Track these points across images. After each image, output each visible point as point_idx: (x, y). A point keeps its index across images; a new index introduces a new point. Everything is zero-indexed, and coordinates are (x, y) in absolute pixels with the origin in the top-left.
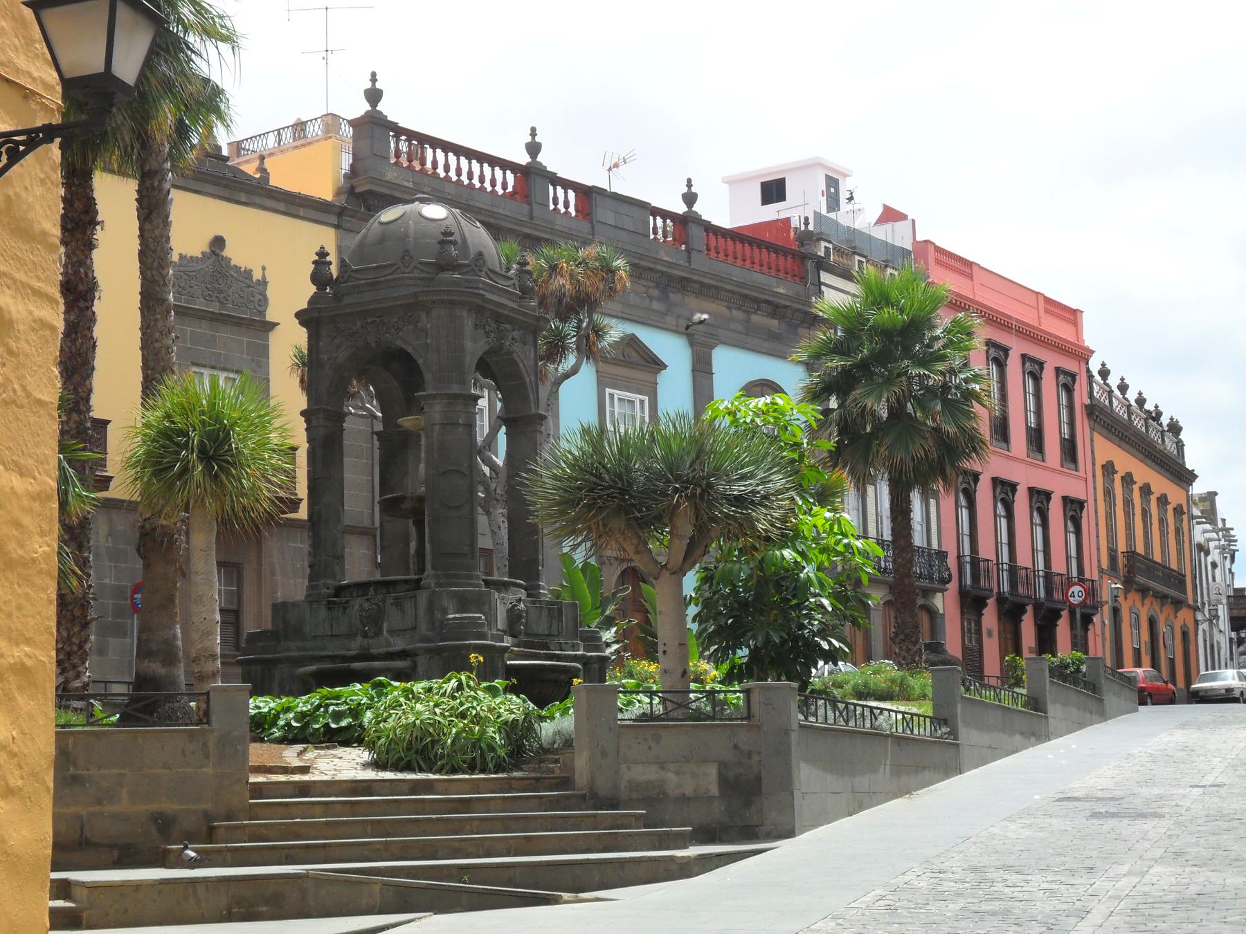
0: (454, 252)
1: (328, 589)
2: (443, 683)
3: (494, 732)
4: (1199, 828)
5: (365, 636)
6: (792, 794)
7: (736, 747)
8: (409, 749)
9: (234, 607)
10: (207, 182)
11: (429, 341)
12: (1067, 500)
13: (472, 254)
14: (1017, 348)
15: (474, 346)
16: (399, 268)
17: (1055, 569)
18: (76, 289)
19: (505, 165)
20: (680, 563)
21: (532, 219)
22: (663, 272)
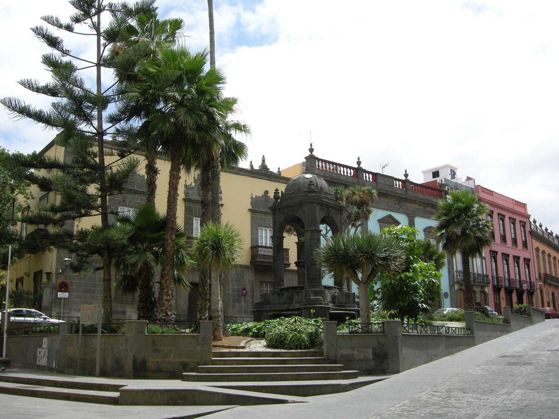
0: (313, 187)
2: (290, 320)
3: (305, 336)
4: (542, 370)
5: (288, 303)
6: (399, 358)
7: (378, 342)
8: (276, 341)
12: (525, 259)
14: (496, 211)
15: (320, 215)
17: (522, 279)
19: (350, 168)
21: (359, 182)
22: (398, 197)
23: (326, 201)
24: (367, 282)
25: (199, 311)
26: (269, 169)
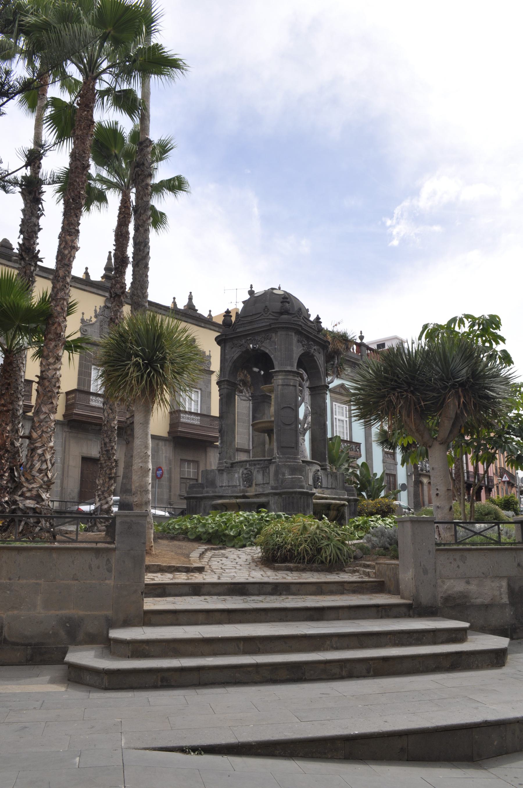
1: (227, 464)
9: (196, 478)
10: (190, 318)
11: (276, 347)
13: (296, 309)
16: (263, 314)
20: (446, 436)
25: (99, 495)
26: (197, 310)
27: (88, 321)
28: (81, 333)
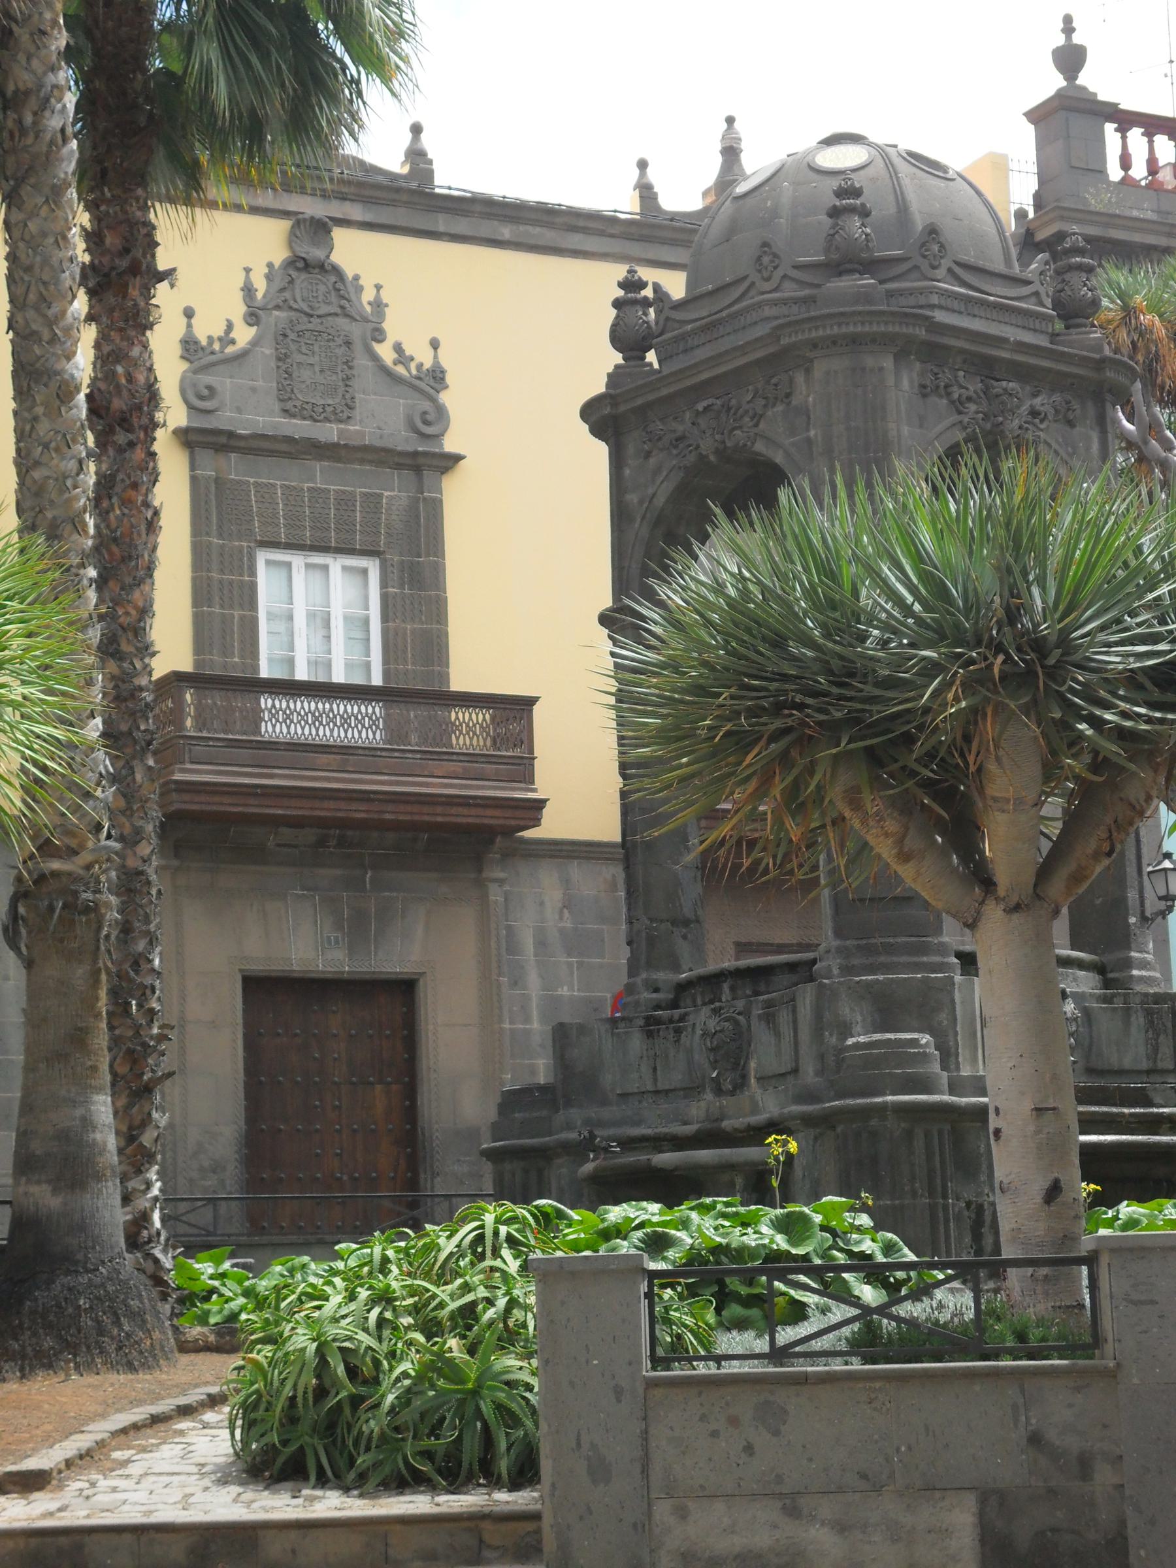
1: (656, 990)
5: (719, 1091)
7: (1035, 1440)
16: (753, 284)
18: (108, 409)
23: (976, 325)
24: (1037, 896)
27: (217, 346)
28: (190, 407)
